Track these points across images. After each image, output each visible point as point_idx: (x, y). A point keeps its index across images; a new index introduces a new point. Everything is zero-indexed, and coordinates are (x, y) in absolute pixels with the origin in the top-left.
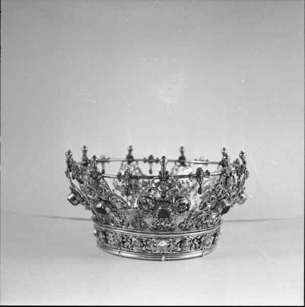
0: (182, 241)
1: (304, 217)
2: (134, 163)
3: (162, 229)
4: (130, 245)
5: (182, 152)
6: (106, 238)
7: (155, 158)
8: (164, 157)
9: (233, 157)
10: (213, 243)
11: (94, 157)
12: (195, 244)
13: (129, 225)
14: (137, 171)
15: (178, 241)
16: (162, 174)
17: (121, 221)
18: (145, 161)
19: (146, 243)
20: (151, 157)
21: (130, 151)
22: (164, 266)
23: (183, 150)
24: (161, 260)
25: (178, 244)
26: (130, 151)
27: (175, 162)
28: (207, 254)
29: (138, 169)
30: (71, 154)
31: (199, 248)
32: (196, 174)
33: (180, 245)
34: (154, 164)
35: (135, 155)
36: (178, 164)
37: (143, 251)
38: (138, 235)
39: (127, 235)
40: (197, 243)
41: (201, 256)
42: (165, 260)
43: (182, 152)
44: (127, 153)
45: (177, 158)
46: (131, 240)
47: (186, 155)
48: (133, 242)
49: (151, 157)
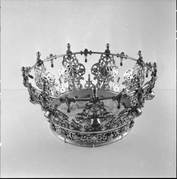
1: (176, 81)
2: (73, 56)
5: (108, 47)
7: (89, 51)
8: (155, 64)
11: (91, 51)
14: (75, 62)
16: (96, 100)
20: (86, 50)
21: (69, 47)
22: (94, 151)
23: (109, 46)
24: (92, 147)
26: (69, 47)
27: (102, 54)
29: (76, 59)
30: (40, 54)
34: (88, 55)
35: (73, 50)
36: (104, 55)
42: (95, 147)
43: (108, 47)
44: (67, 49)
45: (104, 51)
47: (110, 49)
49: (86, 50)
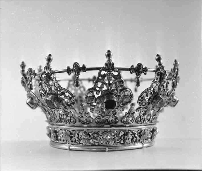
0: (126, 134)
3: (106, 122)
4: (77, 139)
6: (57, 135)
9: (168, 67)
10: (151, 138)
12: (136, 137)
13: (76, 122)
15: (122, 134)
17: (69, 118)
18: (69, 71)
19: (94, 136)
24: (105, 151)
25: (121, 136)
28: (147, 147)
31: (139, 141)
32: (137, 67)
33: (124, 138)
35: (54, 67)
37: (90, 143)
38: (85, 129)
39: (73, 131)
40: (138, 137)
41: (141, 148)
42: (108, 151)
45: (102, 65)
46: (78, 134)
48: (80, 136)
